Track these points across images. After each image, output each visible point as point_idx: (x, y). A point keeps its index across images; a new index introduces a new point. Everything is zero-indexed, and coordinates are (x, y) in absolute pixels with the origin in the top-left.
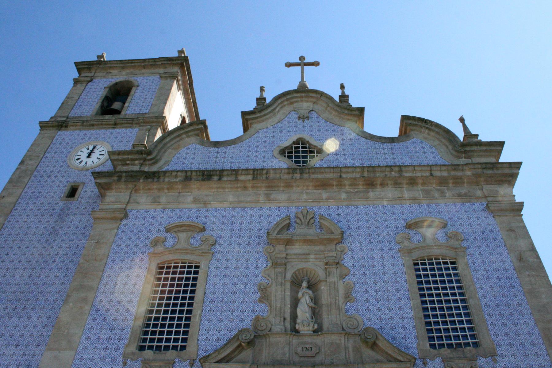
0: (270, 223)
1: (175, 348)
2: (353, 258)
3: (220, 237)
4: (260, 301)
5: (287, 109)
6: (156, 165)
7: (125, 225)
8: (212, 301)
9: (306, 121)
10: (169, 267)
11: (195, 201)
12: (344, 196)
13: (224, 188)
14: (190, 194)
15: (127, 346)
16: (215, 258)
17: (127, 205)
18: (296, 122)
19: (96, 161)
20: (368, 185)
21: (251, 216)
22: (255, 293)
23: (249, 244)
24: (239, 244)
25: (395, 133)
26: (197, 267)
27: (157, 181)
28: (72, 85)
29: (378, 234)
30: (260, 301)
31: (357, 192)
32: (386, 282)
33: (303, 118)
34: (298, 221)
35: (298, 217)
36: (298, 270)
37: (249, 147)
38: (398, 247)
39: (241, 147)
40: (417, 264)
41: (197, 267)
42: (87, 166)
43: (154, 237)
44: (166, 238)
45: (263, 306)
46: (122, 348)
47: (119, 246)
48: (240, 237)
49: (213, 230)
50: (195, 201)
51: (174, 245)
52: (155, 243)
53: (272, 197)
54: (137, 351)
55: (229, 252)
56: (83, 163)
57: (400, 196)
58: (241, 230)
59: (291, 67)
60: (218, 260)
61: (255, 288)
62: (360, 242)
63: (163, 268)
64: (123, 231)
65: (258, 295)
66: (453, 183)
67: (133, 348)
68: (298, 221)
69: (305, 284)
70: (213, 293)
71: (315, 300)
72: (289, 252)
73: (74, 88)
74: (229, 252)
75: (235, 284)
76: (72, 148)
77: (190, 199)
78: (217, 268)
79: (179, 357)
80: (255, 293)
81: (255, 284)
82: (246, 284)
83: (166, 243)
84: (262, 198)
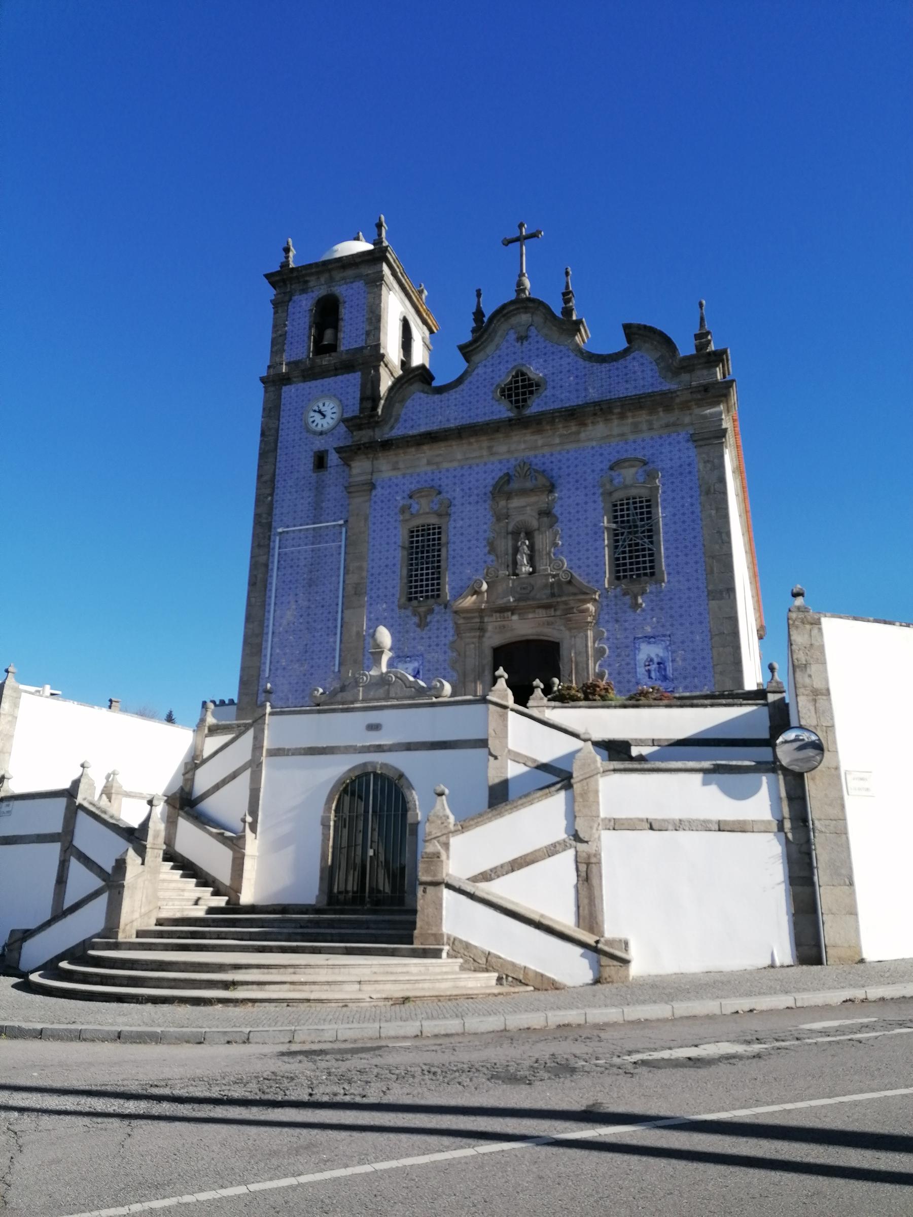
0: (493, 478)
1: (433, 596)
2: (562, 506)
3: (454, 498)
4: (489, 553)
5: (505, 327)
6: (312, 460)
7: (375, 496)
8: (454, 557)
9: (525, 343)
10: (418, 531)
11: (429, 463)
12: (557, 441)
13: (451, 446)
14: (423, 455)
15: (399, 599)
16: (452, 519)
17: (372, 475)
18: (514, 346)
19: (331, 421)
20: (580, 425)
21: (477, 473)
22: (485, 546)
23: (477, 502)
24: (470, 503)
25: (626, 345)
26: (439, 528)
27: (619, 413)
28: (272, 311)
29: (585, 480)
30: (489, 553)
31: (570, 434)
32: (587, 526)
33: (521, 339)
34: (517, 475)
35: (516, 471)
36: (518, 522)
37: (470, 389)
38: (601, 491)
39: (463, 390)
40: (615, 505)
41: (439, 528)
42: (323, 429)
43: (401, 505)
44: (411, 505)
45: (492, 557)
46: (396, 601)
47: (375, 517)
48: (470, 496)
49: (447, 492)
50: (429, 463)
51: (418, 511)
52: (403, 510)
53: (494, 450)
54: (407, 603)
55: (462, 512)
56: (320, 426)
57: (609, 433)
58: (470, 489)
59: (510, 245)
60: (455, 521)
61: (485, 543)
62: (569, 490)
63: (412, 532)
64: (375, 502)
65: (488, 548)
66: (664, 411)
67: (403, 600)
68: (517, 475)
69: (522, 535)
70: (454, 550)
71: (532, 547)
72: (511, 506)
73: (467, 881)
74: (462, 512)
75: (469, 541)
76: (302, 407)
77: (424, 461)
78: (455, 528)
79: (436, 603)
80: (485, 546)
81: (484, 539)
82: (477, 540)
83: (411, 509)
84: (485, 453)
